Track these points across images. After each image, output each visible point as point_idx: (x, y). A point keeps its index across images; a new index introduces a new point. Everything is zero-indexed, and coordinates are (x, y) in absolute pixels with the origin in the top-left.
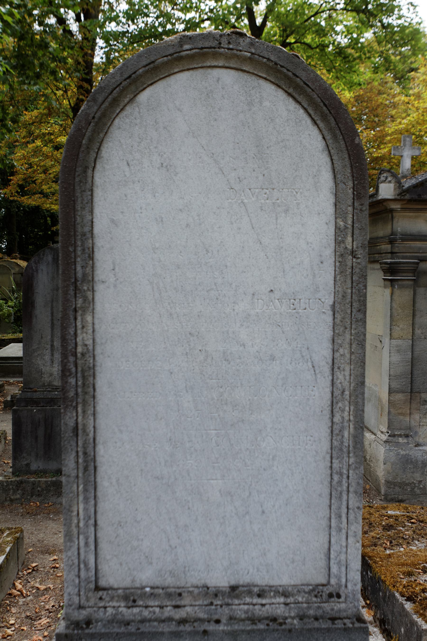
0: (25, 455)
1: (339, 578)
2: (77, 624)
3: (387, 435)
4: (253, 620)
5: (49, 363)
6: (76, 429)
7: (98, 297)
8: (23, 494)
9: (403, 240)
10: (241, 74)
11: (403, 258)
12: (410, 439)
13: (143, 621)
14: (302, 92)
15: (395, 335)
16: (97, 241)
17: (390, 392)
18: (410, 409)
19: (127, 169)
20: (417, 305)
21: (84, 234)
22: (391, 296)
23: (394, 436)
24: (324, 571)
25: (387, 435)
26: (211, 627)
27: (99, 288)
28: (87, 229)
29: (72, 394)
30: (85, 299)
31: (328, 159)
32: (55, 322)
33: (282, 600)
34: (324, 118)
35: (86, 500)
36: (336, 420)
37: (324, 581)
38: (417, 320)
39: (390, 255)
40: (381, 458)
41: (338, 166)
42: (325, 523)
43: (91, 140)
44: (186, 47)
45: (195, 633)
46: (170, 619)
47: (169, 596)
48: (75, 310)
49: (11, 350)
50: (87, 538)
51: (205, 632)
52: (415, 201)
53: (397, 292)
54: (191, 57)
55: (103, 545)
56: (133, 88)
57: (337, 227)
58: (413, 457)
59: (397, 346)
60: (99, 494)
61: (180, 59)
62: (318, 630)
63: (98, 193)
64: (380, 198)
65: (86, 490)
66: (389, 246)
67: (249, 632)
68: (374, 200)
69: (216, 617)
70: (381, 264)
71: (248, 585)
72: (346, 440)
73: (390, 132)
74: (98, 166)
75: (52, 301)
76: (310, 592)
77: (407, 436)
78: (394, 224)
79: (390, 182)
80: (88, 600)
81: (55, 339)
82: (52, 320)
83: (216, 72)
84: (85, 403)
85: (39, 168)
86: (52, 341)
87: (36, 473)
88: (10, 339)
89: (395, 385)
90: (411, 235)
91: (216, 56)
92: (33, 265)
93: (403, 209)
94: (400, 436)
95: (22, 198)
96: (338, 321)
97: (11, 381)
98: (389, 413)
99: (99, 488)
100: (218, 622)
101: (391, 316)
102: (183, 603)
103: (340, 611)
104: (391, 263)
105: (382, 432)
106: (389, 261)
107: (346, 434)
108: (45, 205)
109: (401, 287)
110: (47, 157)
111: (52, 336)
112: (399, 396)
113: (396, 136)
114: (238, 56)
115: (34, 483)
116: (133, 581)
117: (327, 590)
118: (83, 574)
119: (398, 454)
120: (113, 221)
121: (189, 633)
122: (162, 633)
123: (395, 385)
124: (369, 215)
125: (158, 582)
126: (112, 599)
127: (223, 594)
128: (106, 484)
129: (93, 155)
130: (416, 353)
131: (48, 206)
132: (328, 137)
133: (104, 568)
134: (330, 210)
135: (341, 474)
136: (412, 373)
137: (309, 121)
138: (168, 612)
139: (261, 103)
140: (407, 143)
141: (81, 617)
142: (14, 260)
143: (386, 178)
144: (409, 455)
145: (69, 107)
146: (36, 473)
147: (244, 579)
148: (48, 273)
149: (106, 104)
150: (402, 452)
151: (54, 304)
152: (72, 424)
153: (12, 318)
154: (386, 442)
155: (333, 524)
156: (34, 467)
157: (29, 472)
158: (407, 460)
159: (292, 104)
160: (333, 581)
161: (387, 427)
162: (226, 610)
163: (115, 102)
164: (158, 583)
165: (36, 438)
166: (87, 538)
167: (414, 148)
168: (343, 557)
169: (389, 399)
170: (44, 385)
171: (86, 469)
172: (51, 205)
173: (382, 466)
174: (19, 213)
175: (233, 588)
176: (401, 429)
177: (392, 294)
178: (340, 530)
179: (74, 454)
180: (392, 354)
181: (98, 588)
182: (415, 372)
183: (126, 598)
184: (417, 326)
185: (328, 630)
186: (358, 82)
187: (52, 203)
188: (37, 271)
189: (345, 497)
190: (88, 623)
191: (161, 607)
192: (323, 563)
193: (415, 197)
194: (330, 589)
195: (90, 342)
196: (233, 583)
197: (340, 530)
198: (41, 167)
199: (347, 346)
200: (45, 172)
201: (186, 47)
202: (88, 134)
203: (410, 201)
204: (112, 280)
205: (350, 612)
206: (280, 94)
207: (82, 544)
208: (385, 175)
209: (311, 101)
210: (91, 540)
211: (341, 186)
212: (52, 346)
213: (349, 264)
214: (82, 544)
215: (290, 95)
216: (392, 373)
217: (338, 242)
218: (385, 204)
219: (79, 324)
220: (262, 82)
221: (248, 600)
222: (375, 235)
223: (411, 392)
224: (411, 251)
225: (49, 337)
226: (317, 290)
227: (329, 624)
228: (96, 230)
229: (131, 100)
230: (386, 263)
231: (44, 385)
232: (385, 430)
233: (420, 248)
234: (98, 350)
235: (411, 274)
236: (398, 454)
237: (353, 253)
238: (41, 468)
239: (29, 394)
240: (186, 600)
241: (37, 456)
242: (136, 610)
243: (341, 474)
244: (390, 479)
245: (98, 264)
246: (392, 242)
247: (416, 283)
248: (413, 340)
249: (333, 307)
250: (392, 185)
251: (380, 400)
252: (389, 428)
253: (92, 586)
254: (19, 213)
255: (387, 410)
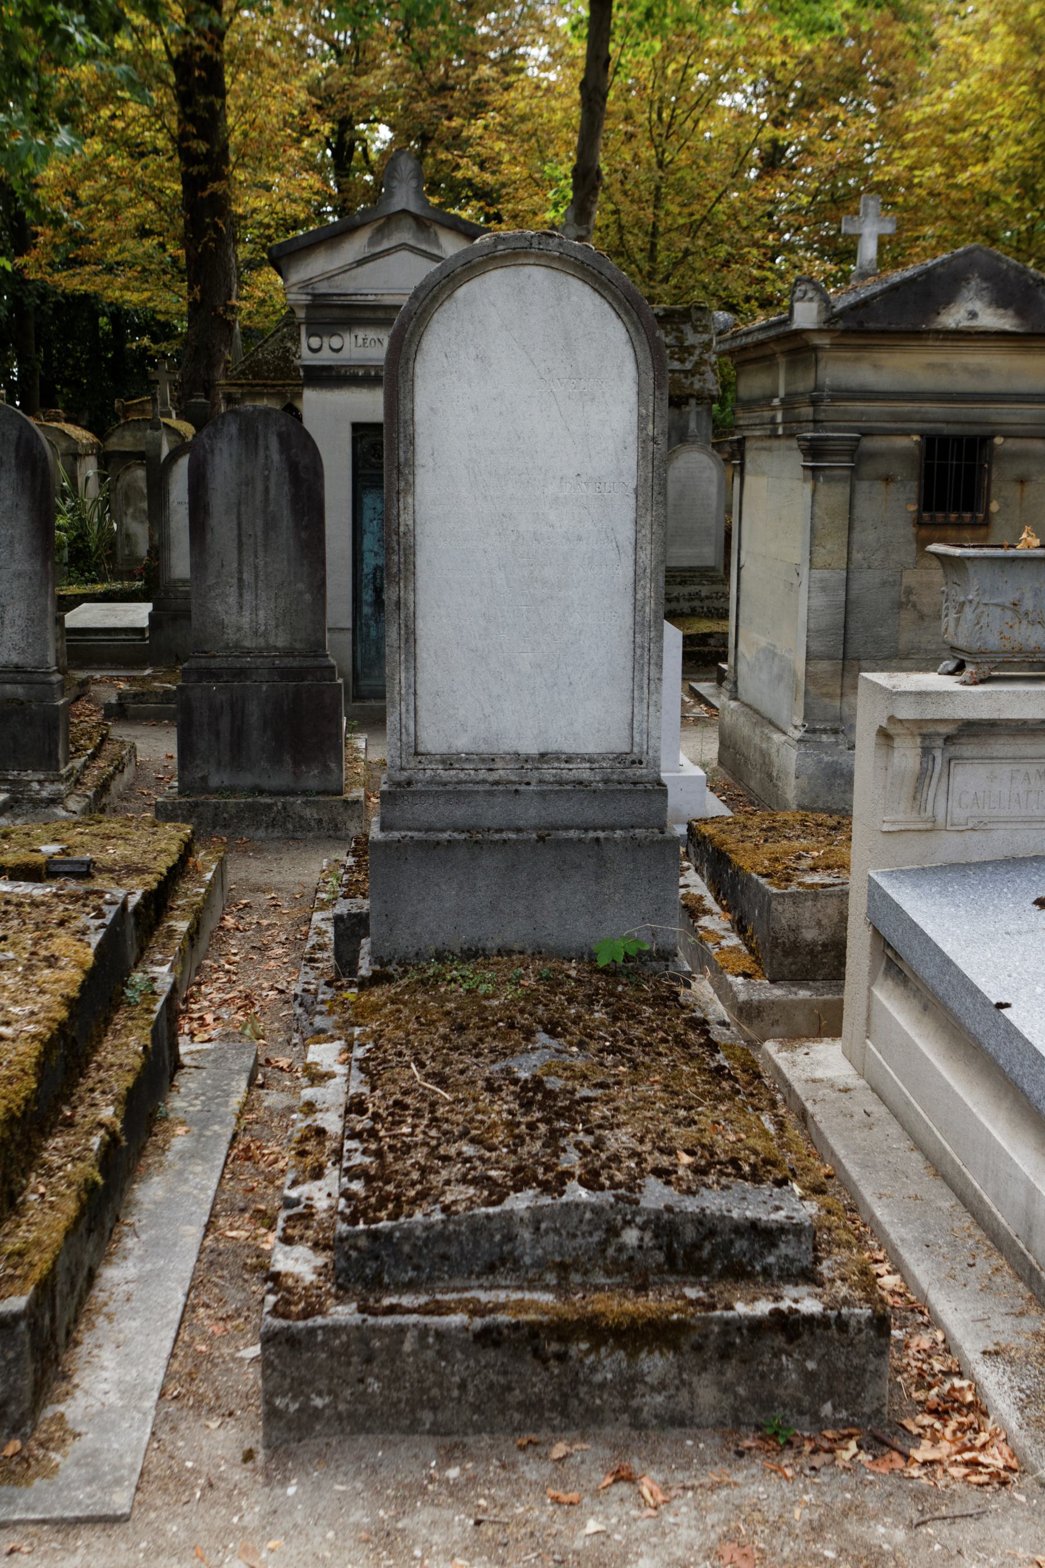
0: (199, 762)
1: (641, 745)
2: (399, 784)
3: (803, 729)
4: (560, 783)
5: (235, 610)
6: (398, 603)
7: (418, 480)
8: (200, 824)
9: (834, 399)
10: (550, 271)
11: (833, 431)
12: (841, 736)
13: (459, 783)
14: (606, 287)
15: (819, 561)
16: (417, 427)
17: (809, 658)
18: (842, 686)
19: (445, 360)
20: (857, 511)
21: (406, 422)
22: (813, 496)
23: (814, 731)
24: (628, 741)
25: (803, 729)
26: (522, 788)
27: (420, 472)
28: (408, 417)
29: (395, 570)
30: (407, 482)
31: (631, 351)
32: (244, 539)
33: (588, 765)
34: (627, 312)
35: (407, 669)
36: (638, 597)
37: (628, 750)
38: (856, 536)
39: (811, 425)
40: (792, 769)
41: (641, 358)
42: (628, 694)
43: (412, 334)
44: (501, 247)
45: (507, 792)
46: (484, 781)
47: (483, 760)
48: (398, 493)
49: (87, 616)
50: (408, 705)
51: (516, 791)
52: (854, 332)
53: (822, 487)
54: (505, 257)
55: (422, 713)
56: (451, 285)
57: (640, 416)
58: (844, 766)
59: (821, 580)
60: (418, 665)
61: (495, 258)
62: (621, 790)
63: (419, 384)
64: (794, 327)
65: (406, 660)
66: (810, 410)
67: (557, 792)
68: (787, 329)
69: (527, 780)
70: (799, 439)
71: (556, 753)
72: (647, 615)
73: (914, 120)
74: (418, 358)
75: (239, 504)
76: (614, 760)
77: (835, 732)
78: (820, 373)
79: (811, 300)
80: (408, 762)
81: (245, 568)
82: (240, 535)
83: (527, 270)
84: (406, 578)
85: (100, 206)
86: (240, 572)
87: (218, 791)
88: (76, 596)
89: (816, 646)
90: (847, 391)
91: (527, 255)
92: (206, 441)
93: (836, 346)
94: (824, 731)
95: (56, 277)
96: (640, 503)
97: (97, 675)
98: (806, 693)
99: (419, 660)
100: (528, 784)
101: (812, 530)
102: (496, 766)
103: (641, 776)
104: (812, 439)
105: (796, 727)
106: (809, 435)
107: (647, 609)
108: (109, 292)
109: (829, 480)
110: (120, 181)
111: (240, 563)
112: (824, 666)
113: (926, 131)
114: (547, 256)
115: (216, 807)
116: (450, 747)
117: (630, 758)
118: (404, 737)
119: (820, 761)
120: (432, 409)
121: (501, 792)
122: (478, 792)
123: (816, 646)
124: (189, 618)
125: (473, 748)
126: (431, 762)
127: (533, 760)
128: (424, 655)
129: (414, 347)
130: (853, 593)
131: (117, 294)
132: (631, 330)
133: (423, 735)
134: (633, 398)
135: (643, 648)
136: (845, 627)
137: (613, 314)
138: (483, 774)
139: (569, 298)
140: (870, 210)
141: (403, 778)
142: (55, 424)
143: (805, 293)
144: (837, 763)
145: (165, 58)
146: (218, 791)
147: (553, 747)
148: (231, 455)
149: (427, 301)
150: (827, 759)
151: (243, 509)
152: (394, 598)
153: (66, 553)
154: (800, 741)
155: (636, 696)
156: (214, 781)
157: (206, 790)
158: (835, 772)
159: (597, 299)
160: (636, 750)
161: (802, 716)
162: (536, 773)
163: (435, 298)
164: (472, 750)
165: (217, 734)
166: (408, 705)
167: (882, 220)
168: (644, 725)
169: (806, 669)
170: (227, 647)
171: (407, 641)
172: (125, 292)
173: (793, 782)
174: (43, 307)
175: (543, 755)
176: (826, 720)
177: (814, 492)
178: (642, 700)
179: (395, 628)
180: (813, 595)
181: (417, 754)
182: (852, 625)
183: (443, 762)
184: (855, 547)
185: (630, 791)
186: (827, 24)
187: (127, 288)
188: (212, 451)
189: (646, 669)
190: (409, 783)
191: (476, 770)
192: (626, 733)
193: (853, 325)
194: (634, 757)
195: (411, 523)
196: (542, 750)
197: (642, 700)
198: (105, 204)
199: (648, 527)
200: (114, 215)
201: (501, 247)
202: (410, 328)
203: (845, 332)
204: (431, 464)
205: (651, 777)
206: (587, 289)
207: (403, 710)
208: (803, 287)
209: (616, 297)
210: (412, 707)
211: (643, 375)
212: (240, 580)
213: (650, 449)
214: (403, 710)
215: (595, 290)
216: (812, 626)
217: (641, 429)
218: (804, 336)
219: (401, 505)
220: (570, 278)
221: (556, 765)
222: (793, 388)
223: (844, 659)
224: (847, 418)
225: (235, 565)
226: (621, 474)
227: (632, 787)
228: (416, 418)
229: (449, 296)
230: (805, 439)
231: (227, 647)
232: (799, 722)
233: (862, 413)
234: (418, 530)
235: (847, 458)
236: (820, 761)
237: (654, 440)
238: (226, 783)
239: (203, 661)
240: (499, 764)
241: (219, 763)
242: (452, 772)
243: (643, 648)
244: (806, 802)
245: (418, 450)
246: (815, 402)
247: (855, 473)
248: (848, 569)
249: (636, 490)
250: (814, 306)
251: (794, 674)
252: (805, 718)
253: (412, 751)
254: (43, 307)
255: (802, 688)
